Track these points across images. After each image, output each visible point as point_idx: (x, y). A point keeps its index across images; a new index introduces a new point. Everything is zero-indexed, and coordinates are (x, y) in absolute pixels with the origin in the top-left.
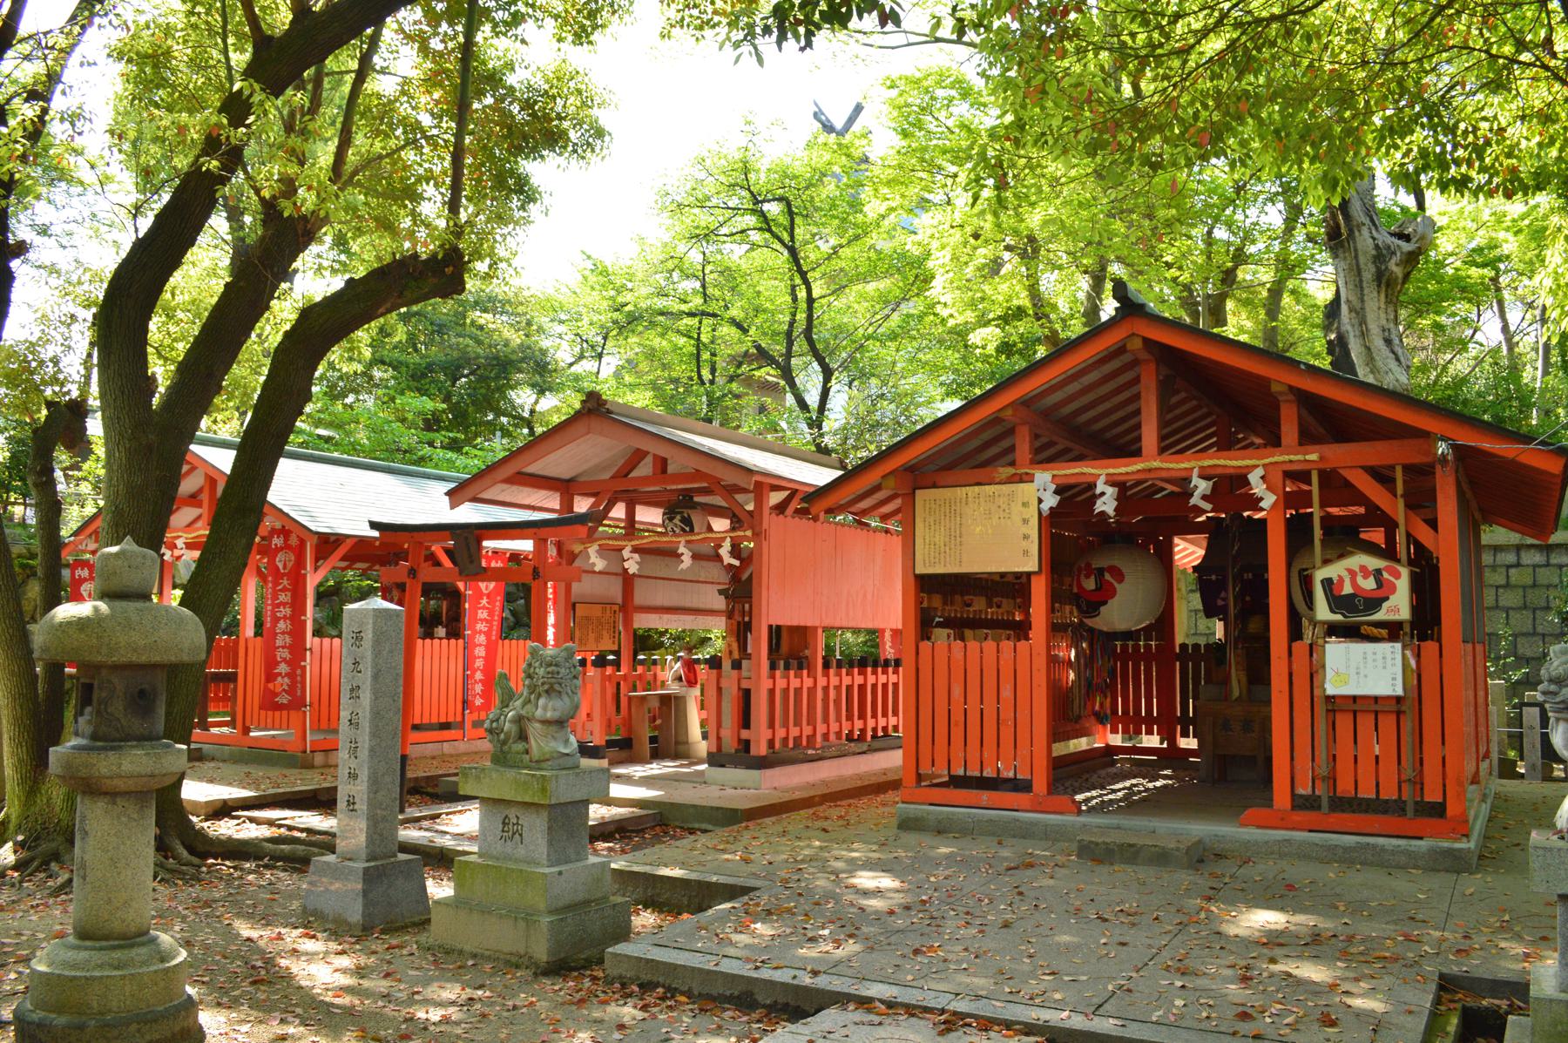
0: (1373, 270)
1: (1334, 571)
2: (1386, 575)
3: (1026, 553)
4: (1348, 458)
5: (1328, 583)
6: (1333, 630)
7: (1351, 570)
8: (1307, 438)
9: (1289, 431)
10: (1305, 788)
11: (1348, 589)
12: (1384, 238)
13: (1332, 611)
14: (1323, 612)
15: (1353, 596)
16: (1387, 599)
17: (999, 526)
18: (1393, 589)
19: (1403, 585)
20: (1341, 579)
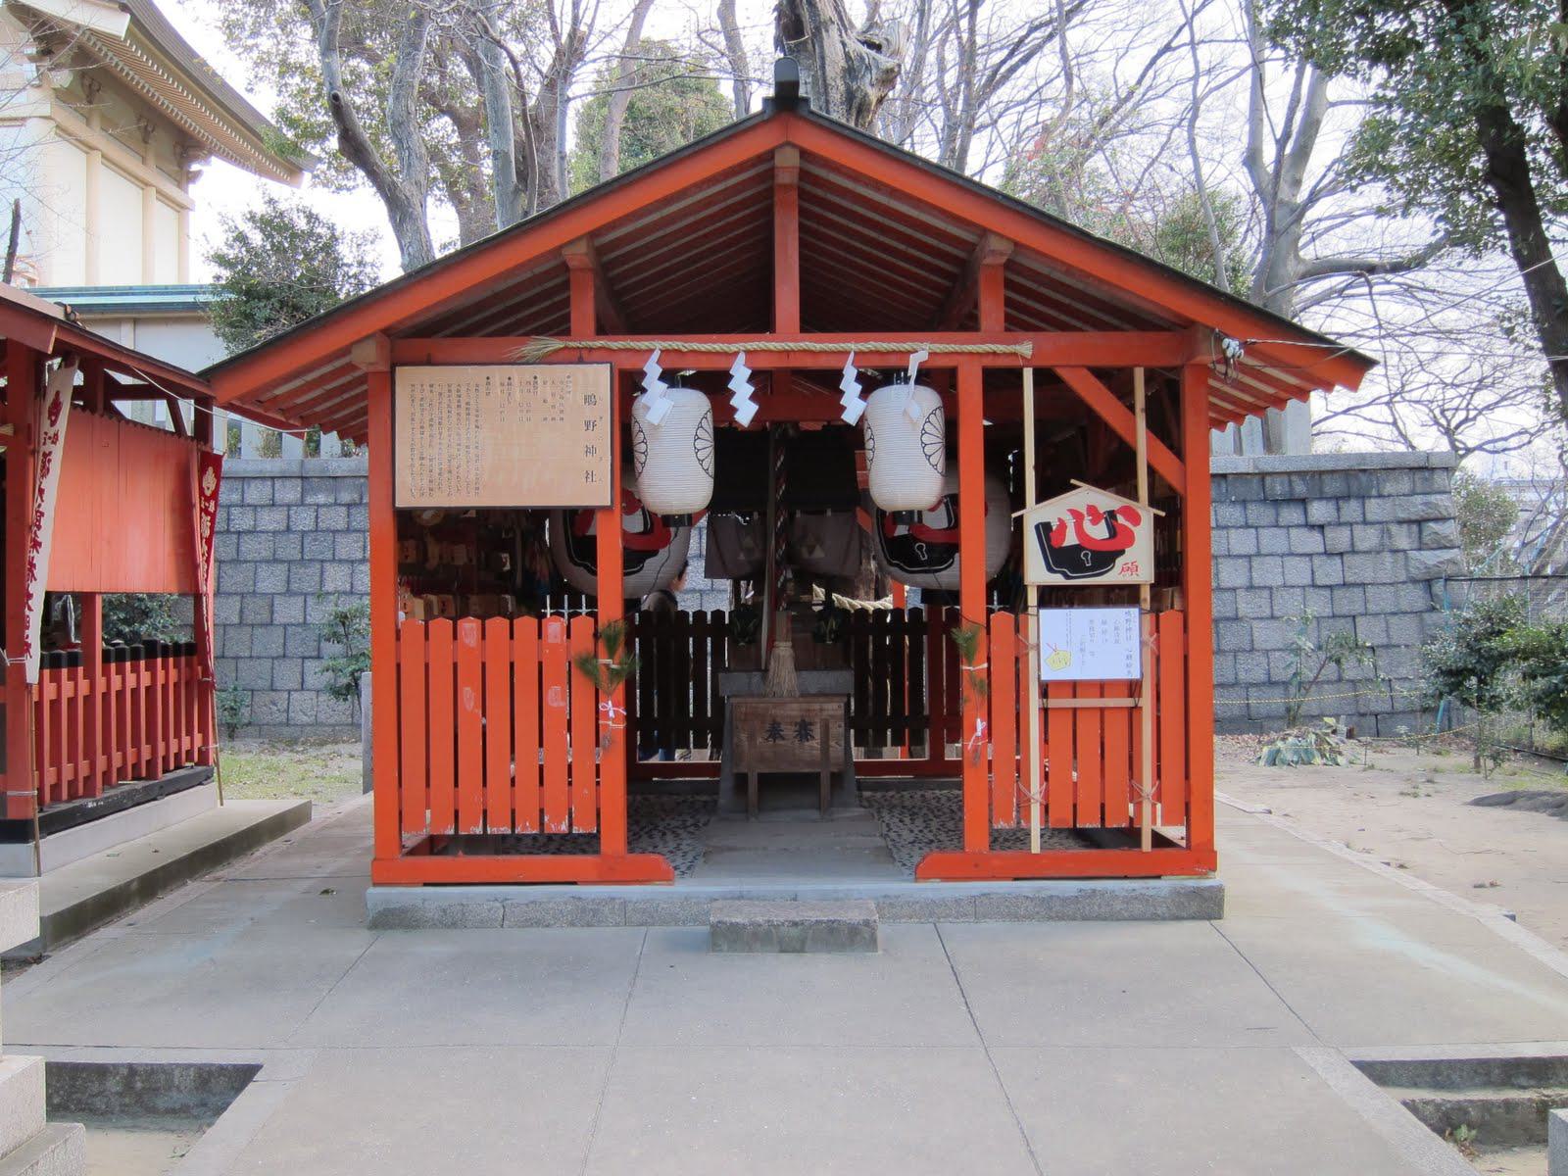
0: (842, 88)
1: (1054, 511)
2: (1121, 519)
3: (589, 475)
4: (1074, 355)
5: (1044, 529)
6: (1051, 597)
7: (1078, 509)
8: (1017, 322)
9: (991, 309)
10: (1007, 818)
11: (1071, 539)
12: (856, 47)
13: (1050, 570)
14: (1037, 572)
15: (1077, 548)
16: (1121, 552)
17: (516, 435)
18: (1130, 539)
19: (1144, 536)
20: (1063, 525)
